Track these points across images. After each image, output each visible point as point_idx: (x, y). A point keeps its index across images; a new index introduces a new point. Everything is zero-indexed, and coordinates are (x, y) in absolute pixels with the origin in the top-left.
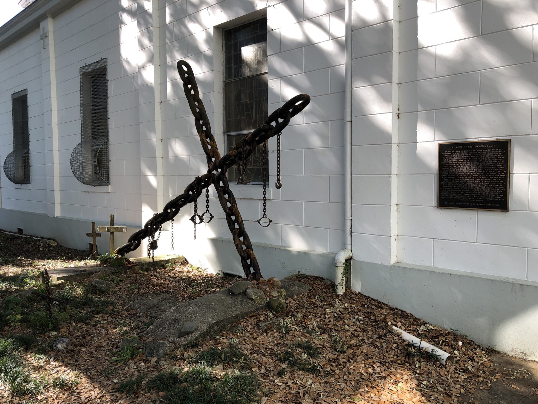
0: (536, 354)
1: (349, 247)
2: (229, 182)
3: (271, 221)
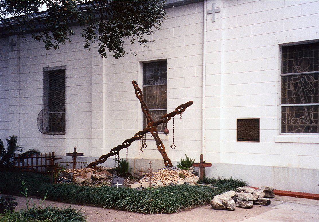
2: (158, 133)
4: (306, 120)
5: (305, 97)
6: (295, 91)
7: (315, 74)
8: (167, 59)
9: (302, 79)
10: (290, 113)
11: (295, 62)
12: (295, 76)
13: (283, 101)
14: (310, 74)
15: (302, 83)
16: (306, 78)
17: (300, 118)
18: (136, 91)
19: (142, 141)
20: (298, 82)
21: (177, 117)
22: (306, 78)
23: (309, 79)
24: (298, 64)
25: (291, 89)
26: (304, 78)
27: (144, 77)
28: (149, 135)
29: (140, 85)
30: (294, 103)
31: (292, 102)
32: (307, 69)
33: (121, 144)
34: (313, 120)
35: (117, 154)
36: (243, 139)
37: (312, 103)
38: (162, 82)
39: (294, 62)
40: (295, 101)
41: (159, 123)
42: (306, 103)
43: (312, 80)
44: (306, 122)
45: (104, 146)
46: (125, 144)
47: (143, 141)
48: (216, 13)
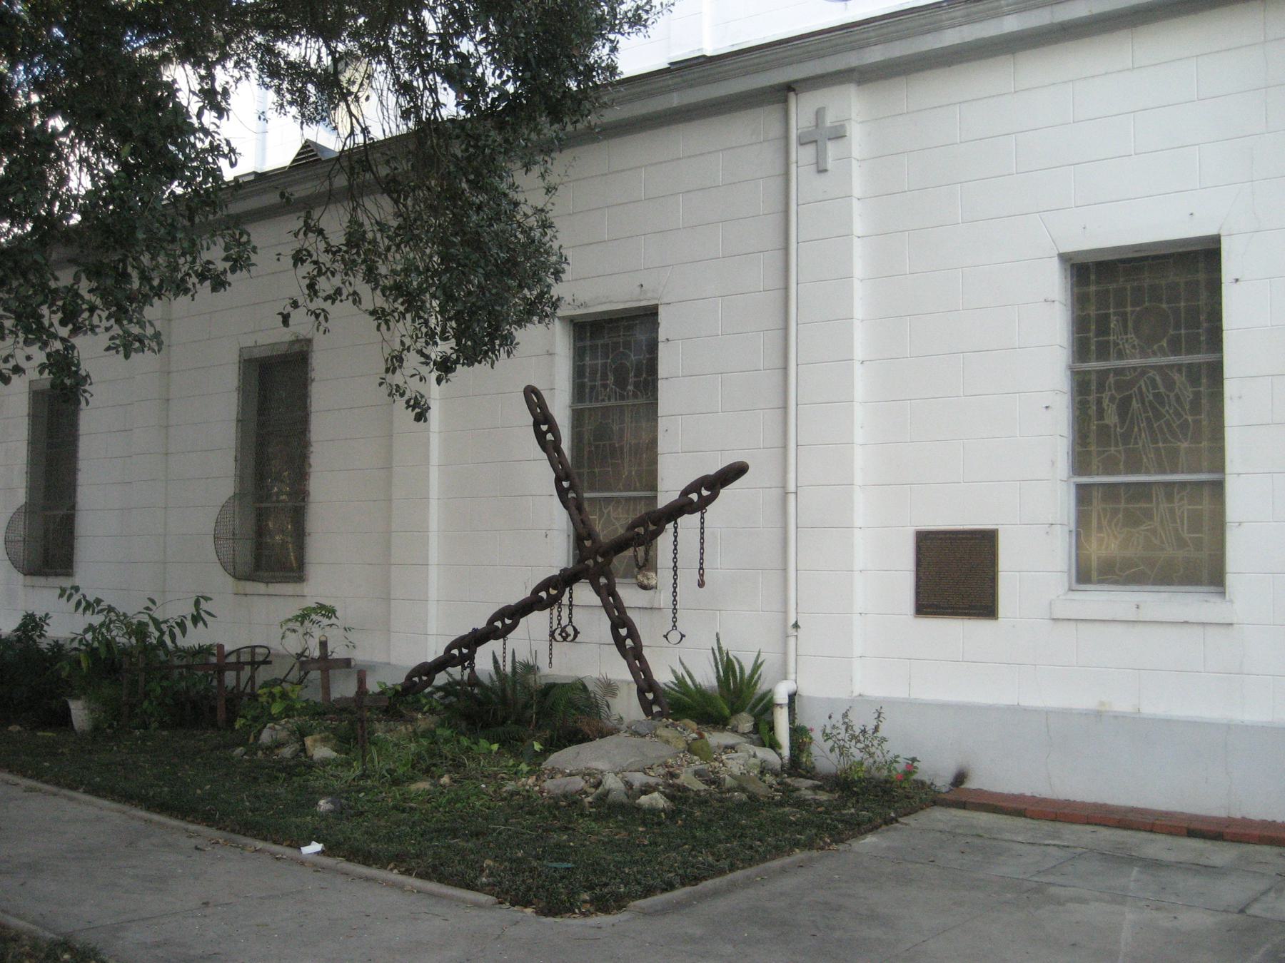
0: (624, 71)
1: (792, 676)
2: (617, 580)
3: (683, 636)
4: (1161, 536)
5: (1157, 449)
6: (1121, 428)
7: (1190, 366)
8: (657, 305)
9: (1146, 383)
10: (1104, 510)
11: (1117, 321)
12: (1119, 372)
13: (1080, 462)
14: (1171, 367)
15: (1146, 399)
16: (1158, 378)
17: (1142, 528)
18: (536, 425)
19: (555, 612)
20: (1131, 395)
21: (688, 522)
22: (1158, 378)
23: (1170, 385)
24: (1130, 324)
25: (1106, 422)
26: (1153, 381)
27: (579, 372)
28: (584, 593)
29: (560, 407)
30: (1119, 473)
31: (1110, 468)
32: (1161, 348)
33: (481, 624)
34: (1186, 535)
35: (471, 657)
36: (938, 607)
37: (1183, 472)
38: (641, 392)
39: (1113, 319)
40: (1121, 466)
41: (620, 546)
42: (1164, 472)
43: (1179, 388)
44: (1162, 542)
45: (433, 627)
46: (496, 624)
47: (559, 621)
48: (829, 139)
